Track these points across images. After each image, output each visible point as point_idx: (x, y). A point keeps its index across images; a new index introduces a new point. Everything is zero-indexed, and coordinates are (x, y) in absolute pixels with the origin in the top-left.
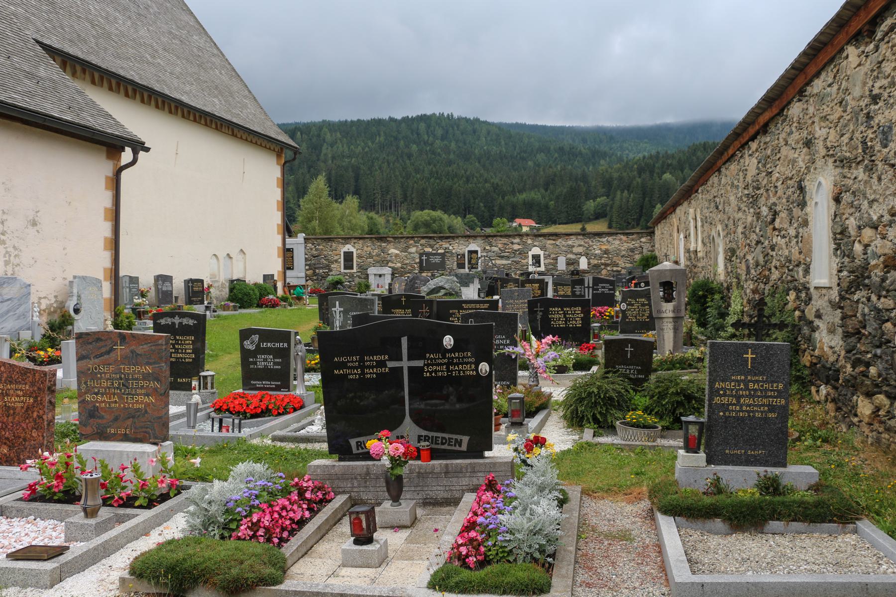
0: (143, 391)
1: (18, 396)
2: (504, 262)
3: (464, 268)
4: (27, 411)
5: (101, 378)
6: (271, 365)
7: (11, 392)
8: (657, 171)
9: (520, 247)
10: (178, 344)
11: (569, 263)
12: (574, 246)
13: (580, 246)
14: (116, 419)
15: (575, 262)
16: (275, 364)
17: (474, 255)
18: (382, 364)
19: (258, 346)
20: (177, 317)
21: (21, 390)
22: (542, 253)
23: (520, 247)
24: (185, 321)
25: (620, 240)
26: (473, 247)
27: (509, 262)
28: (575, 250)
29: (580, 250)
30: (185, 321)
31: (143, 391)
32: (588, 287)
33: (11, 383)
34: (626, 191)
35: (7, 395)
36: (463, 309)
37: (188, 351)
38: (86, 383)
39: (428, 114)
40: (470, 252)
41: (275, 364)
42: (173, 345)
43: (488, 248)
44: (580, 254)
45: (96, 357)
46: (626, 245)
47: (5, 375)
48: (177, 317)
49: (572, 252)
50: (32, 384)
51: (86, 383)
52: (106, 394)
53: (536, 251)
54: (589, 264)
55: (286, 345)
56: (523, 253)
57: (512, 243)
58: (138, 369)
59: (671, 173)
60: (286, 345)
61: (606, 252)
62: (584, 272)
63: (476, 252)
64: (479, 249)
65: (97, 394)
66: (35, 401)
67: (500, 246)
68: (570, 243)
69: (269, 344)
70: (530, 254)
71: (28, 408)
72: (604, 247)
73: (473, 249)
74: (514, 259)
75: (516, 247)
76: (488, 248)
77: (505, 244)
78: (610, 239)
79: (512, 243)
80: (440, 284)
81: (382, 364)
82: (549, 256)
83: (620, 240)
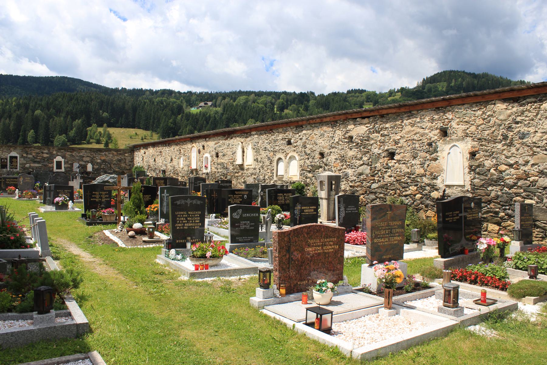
0: (397, 234)
1: (331, 245)
2: (37, 165)
3: (57, 169)
4: (335, 253)
5: (381, 230)
6: (248, 227)
7: (327, 243)
8: (30, 107)
9: (48, 156)
10: (190, 217)
11: (81, 166)
12: (84, 157)
13: (88, 156)
14: (386, 250)
15: (85, 167)
16: (251, 226)
17: (14, 160)
18: (457, 215)
19: (241, 216)
20: (189, 200)
21: (332, 241)
22: (63, 160)
23: (48, 156)
24: (194, 202)
25: (113, 154)
26: (14, 154)
27: (40, 165)
28: (85, 159)
29: (88, 159)
30: (194, 202)
31: (397, 234)
32: (192, 183)
33: (327, 238)
34: (8, 119)
35: (325, 245)
36: (235, 194)
37: (197, 221)
38: (375, 233)
39: (326, 94)
40: (11, 158)
41: (251, 226)
42: (186, 218)
43: (25, 155)
44: (88, 162)
45: (379, 219)
46: (116, 158)
47: (324, 233)
48: (189, 200)
49: (82, 160)
50: (338, 238)
51: (375, 233)
52: (383, 237)
53: (59, 158)
54: (93, 168)
55: (257, 215)
56: (50, 159)
57: (43, 153)
58: (395, 223)
59: (41, 110)
60: (257, 215)
61: (104, 161)
62: (90, 173)
63: (16, 157)
64: (18, 156)
65: (379, 238)
66: (339, 247)
67: (34, 154)
68: (81, 154)
69: (248, 215)
70: (55, 160)
71: (336, 252)
72: (103, 158)
73: (14, 155)
74: (44, 164)
75: (45, 155)
76: (25, 155)
77: (37, 153)
78: (107, 153)
79: (43, 153)
80: (106, 179)
81: (457, 215)
82: (68, 162)
83: (113, 154)
